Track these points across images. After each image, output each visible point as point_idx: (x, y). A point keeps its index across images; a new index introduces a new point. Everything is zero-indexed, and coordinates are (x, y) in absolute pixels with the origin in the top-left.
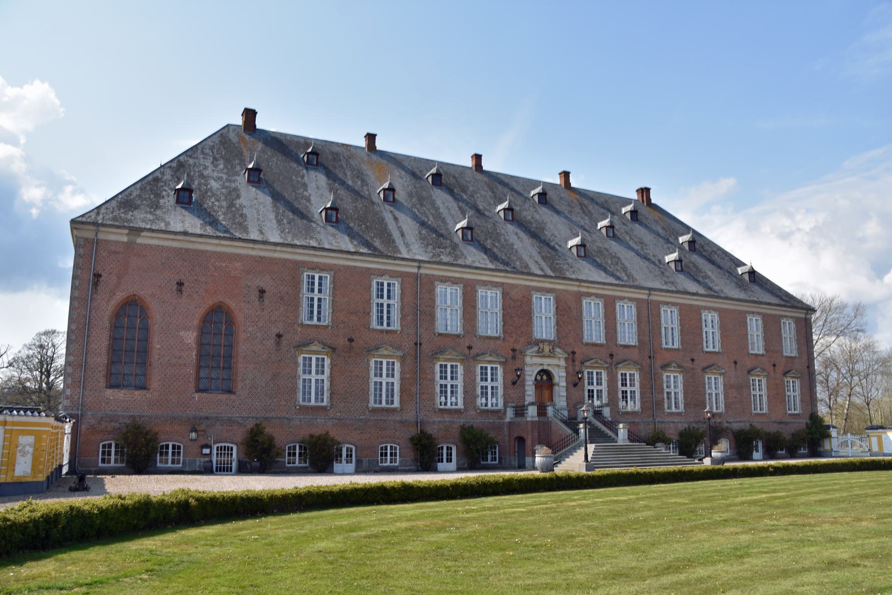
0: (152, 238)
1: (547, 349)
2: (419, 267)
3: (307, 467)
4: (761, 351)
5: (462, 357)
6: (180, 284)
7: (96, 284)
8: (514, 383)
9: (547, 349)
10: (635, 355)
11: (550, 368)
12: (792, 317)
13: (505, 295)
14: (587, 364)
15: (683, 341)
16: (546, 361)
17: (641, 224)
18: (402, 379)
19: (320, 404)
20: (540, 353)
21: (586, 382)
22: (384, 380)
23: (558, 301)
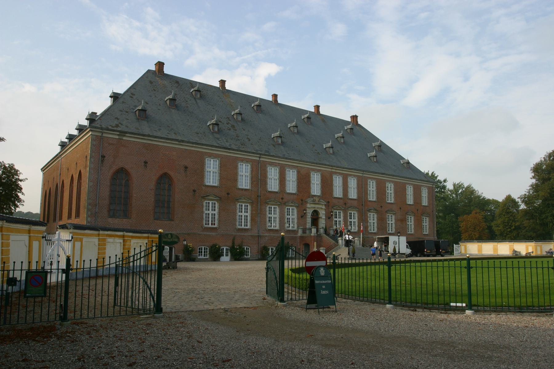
0: (192, 147)
1: (317, 199)
2: (260, 157)
3: (207, 259)
4: (294, 191)
5: (218, 199)
6: (146, 163)
7: (102, 161)
8: (302, 217)
9: (317, 199)
10: (355, 203)
11: (318, 210)
12: (426, 186)
13: (298, 172)
14: (335, 208)
15: (377, 197)
16: (317, 206)
17: (354, 135)
18: (252, 214)
19: (213, 226)
20: (314, 202)
21: (334, 216)
22: (211, 212)
23: (322, 176)
